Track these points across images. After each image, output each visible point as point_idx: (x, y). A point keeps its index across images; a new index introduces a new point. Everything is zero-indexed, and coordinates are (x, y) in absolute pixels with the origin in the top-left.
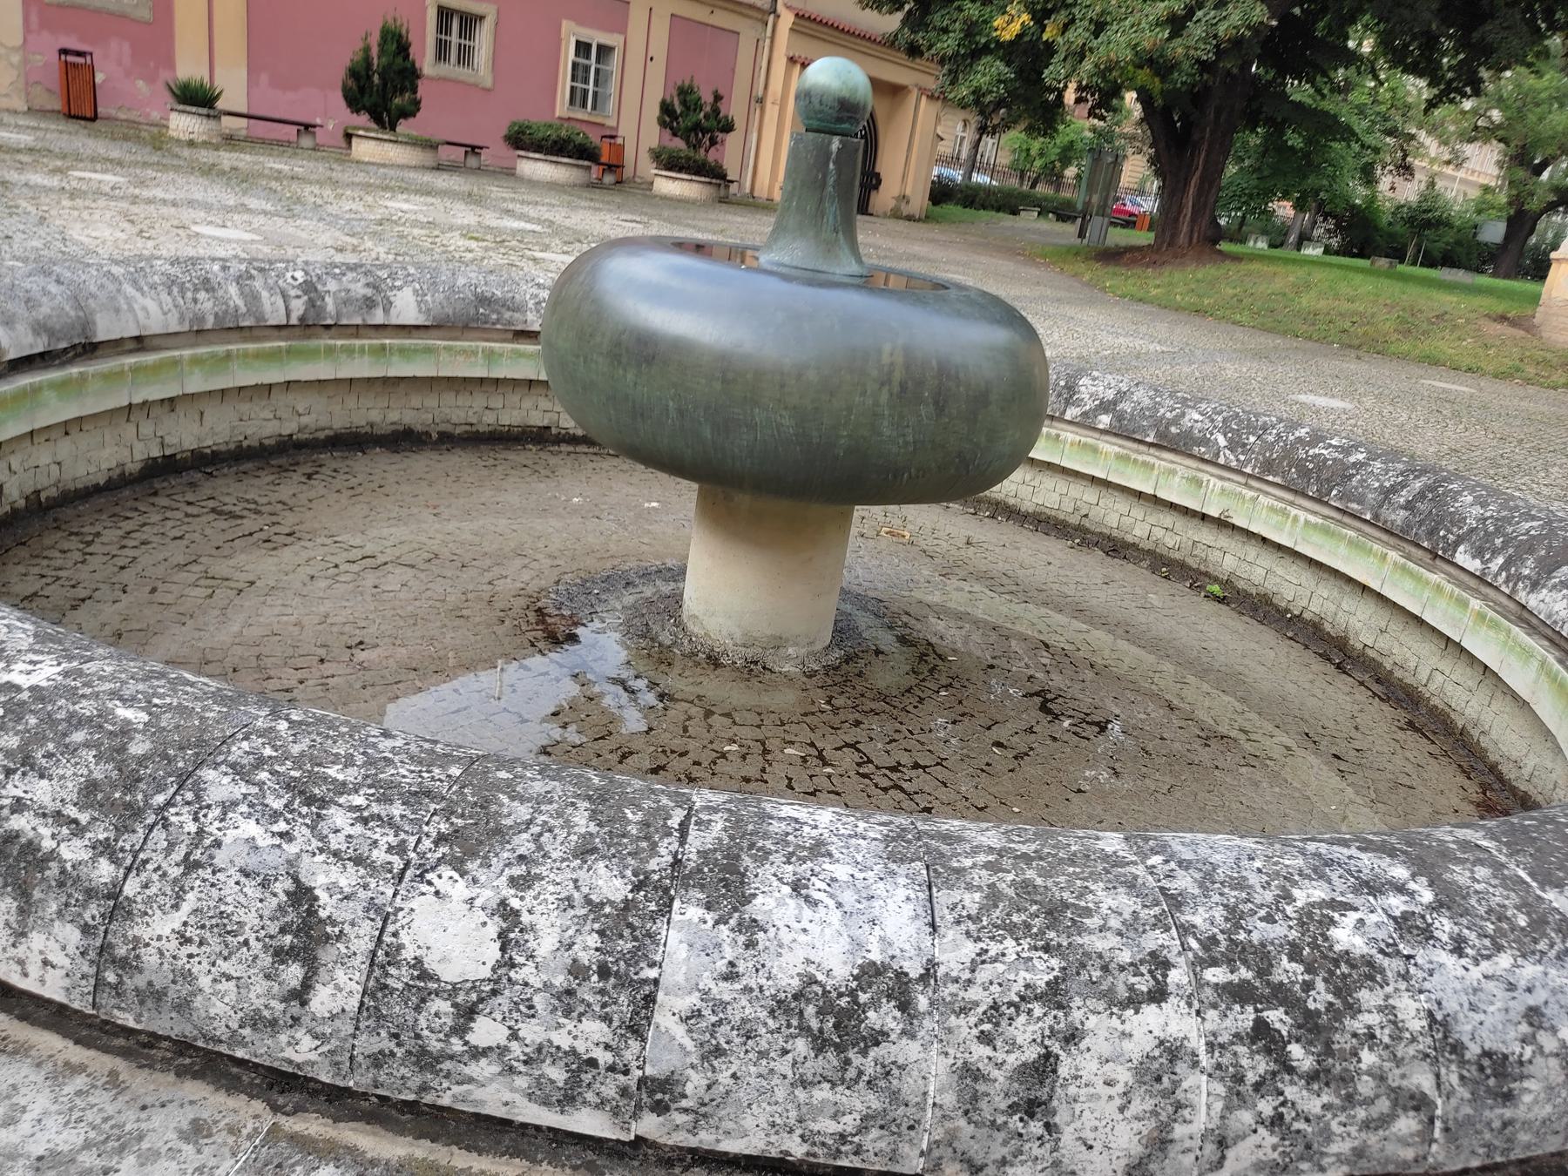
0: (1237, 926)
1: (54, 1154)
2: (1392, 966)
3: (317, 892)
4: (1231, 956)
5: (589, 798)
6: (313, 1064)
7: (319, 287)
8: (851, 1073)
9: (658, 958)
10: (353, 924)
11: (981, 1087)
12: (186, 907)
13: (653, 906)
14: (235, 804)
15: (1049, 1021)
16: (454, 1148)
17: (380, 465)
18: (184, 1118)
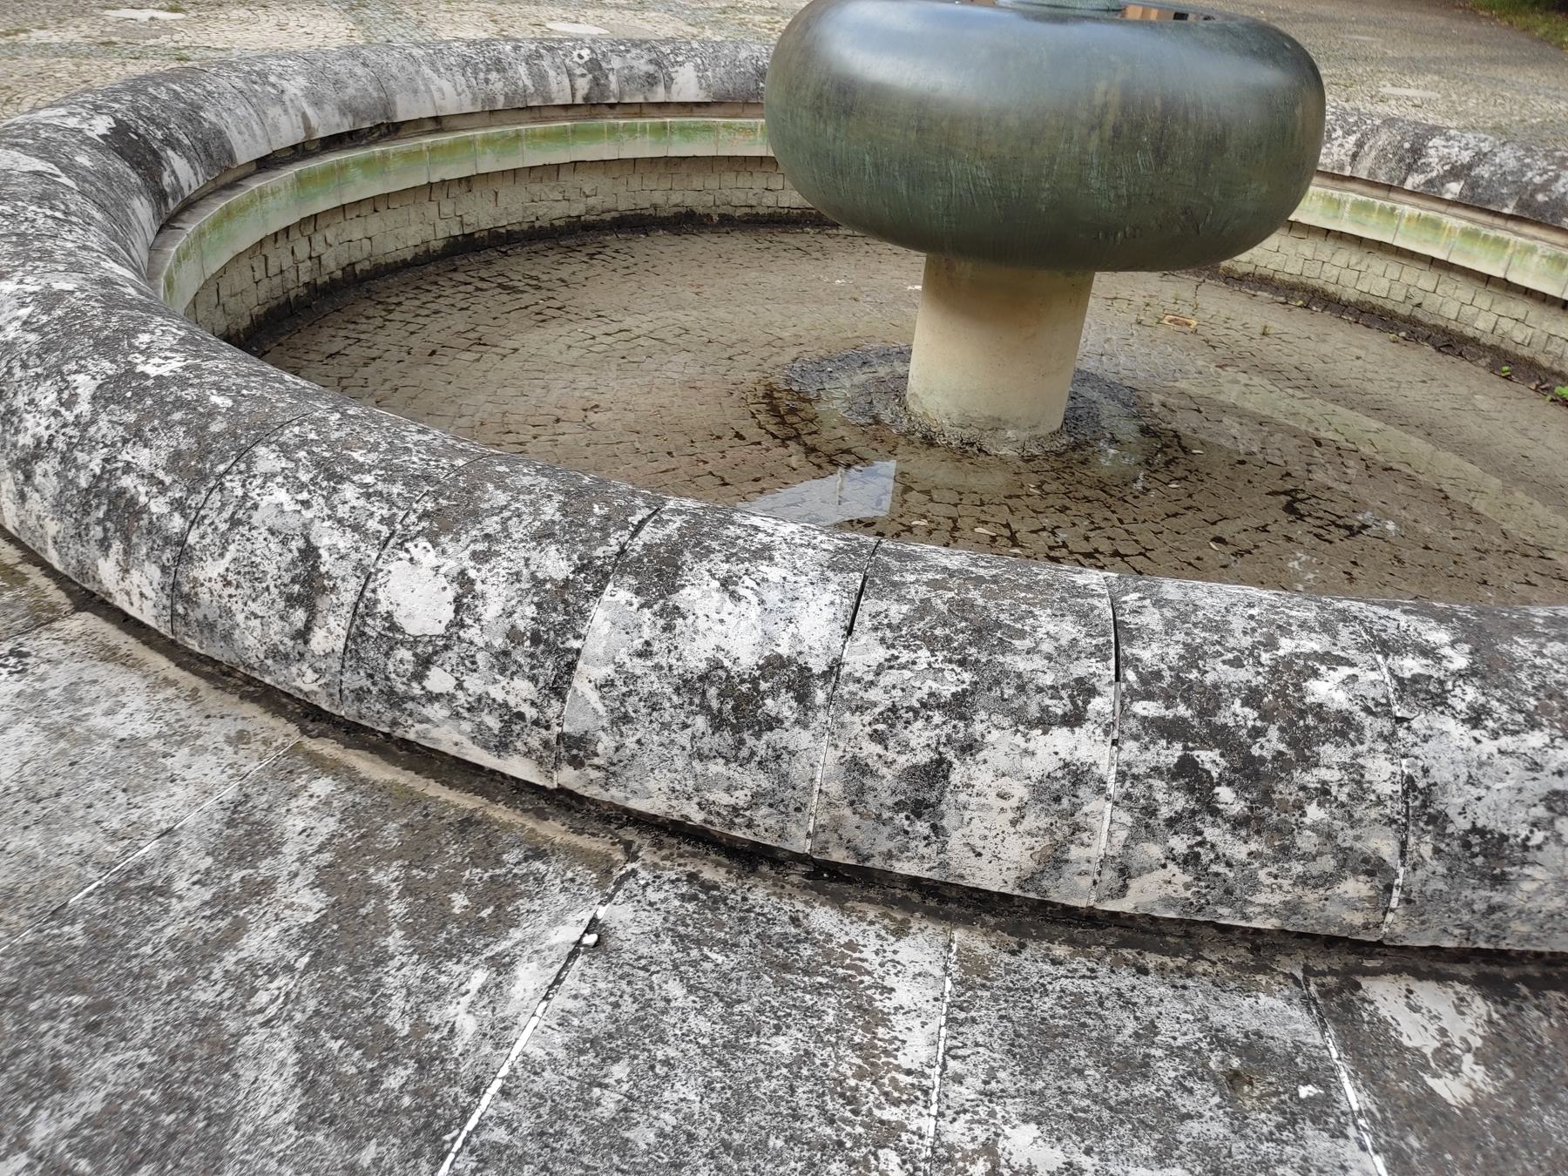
0: (1193, 665)
1: (133, 738)
2: (1374, 726)
3: (321, 551)
4: (1172, 692)
5: (567, 493)
6: (316, 693)
7: (604, 65)
8: (744, 753)
9: (583, 631)
10: (343, 580)
11: (868, 782)
12: (229, 556)
13: (589, 588)
14: (274, 475)
15: (948, 729)
16: (432, 781)
17: (662, 246)
18: (232, 728)
